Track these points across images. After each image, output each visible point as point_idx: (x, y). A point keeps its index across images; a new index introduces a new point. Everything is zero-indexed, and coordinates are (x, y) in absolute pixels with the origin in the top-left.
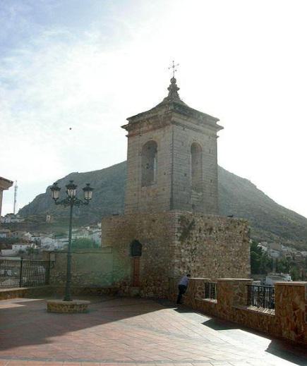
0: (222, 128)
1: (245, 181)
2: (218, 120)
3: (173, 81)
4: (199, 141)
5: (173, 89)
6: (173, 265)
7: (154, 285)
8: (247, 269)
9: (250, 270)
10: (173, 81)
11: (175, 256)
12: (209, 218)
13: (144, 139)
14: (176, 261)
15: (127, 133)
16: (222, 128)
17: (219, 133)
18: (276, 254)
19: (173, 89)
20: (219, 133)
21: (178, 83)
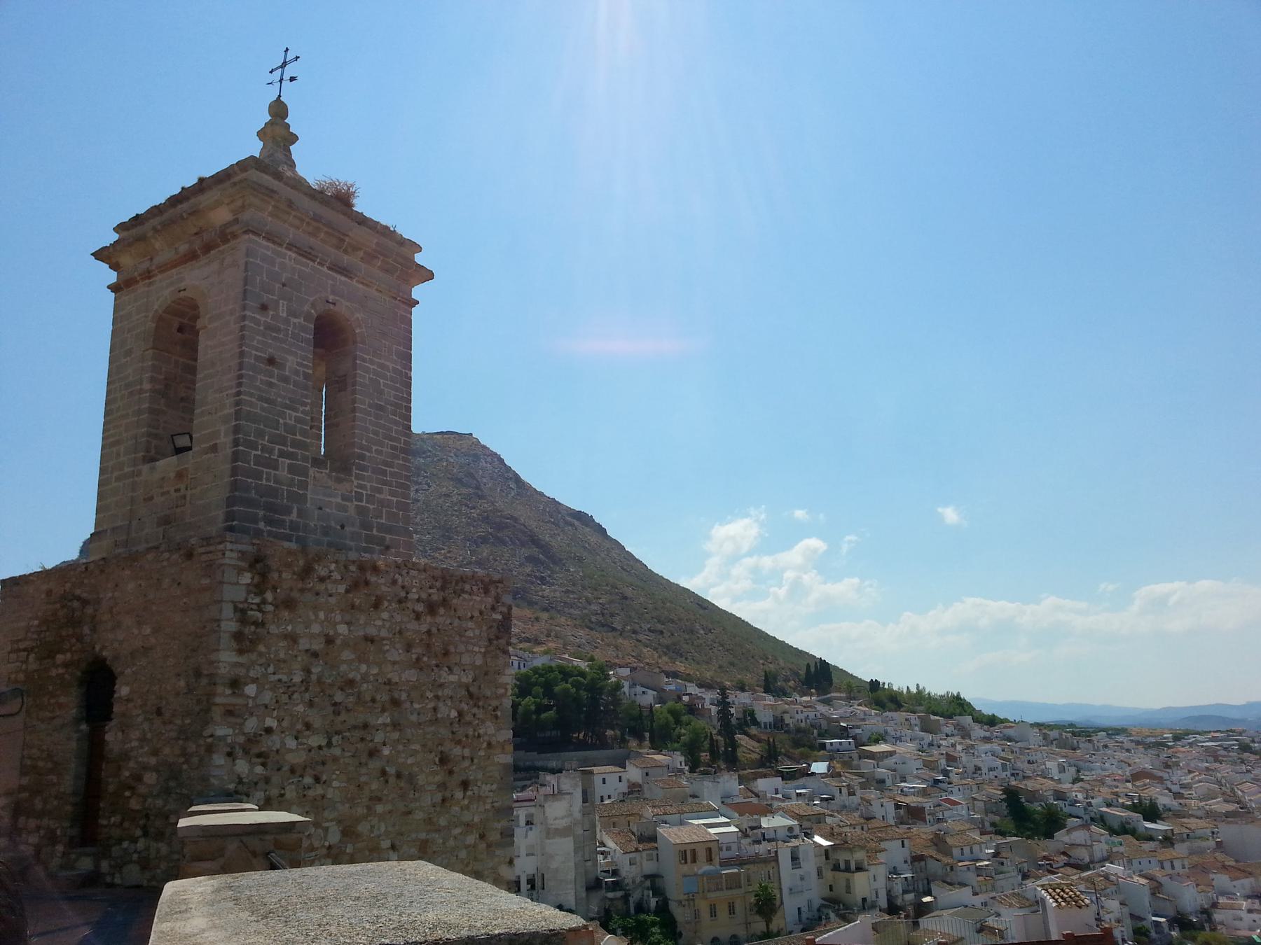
0: (429, 275)
1: (583, 519)
2: (419, 249)
3: (279, 110)
4: (343, 308)
5: (278, 131)
6: (210, 749)
7: (146, 834)
8: (502, 745)
9: (510, 748)
10: (279, 110)
11: (217, 713)
12: (537, 619)
13: (161, 293)
14: (221, 731)
15: (112, 277)
16: (429, 275)
17: (417, 292)
18: (648, 698)
19: (278, 131)
20: (417, 292)
21: (294, 122)
